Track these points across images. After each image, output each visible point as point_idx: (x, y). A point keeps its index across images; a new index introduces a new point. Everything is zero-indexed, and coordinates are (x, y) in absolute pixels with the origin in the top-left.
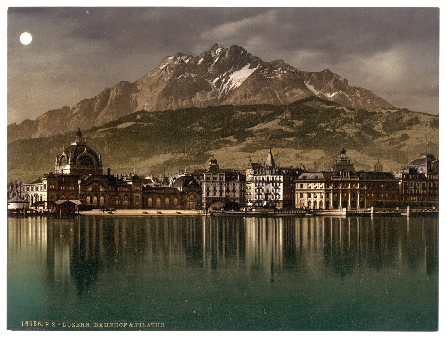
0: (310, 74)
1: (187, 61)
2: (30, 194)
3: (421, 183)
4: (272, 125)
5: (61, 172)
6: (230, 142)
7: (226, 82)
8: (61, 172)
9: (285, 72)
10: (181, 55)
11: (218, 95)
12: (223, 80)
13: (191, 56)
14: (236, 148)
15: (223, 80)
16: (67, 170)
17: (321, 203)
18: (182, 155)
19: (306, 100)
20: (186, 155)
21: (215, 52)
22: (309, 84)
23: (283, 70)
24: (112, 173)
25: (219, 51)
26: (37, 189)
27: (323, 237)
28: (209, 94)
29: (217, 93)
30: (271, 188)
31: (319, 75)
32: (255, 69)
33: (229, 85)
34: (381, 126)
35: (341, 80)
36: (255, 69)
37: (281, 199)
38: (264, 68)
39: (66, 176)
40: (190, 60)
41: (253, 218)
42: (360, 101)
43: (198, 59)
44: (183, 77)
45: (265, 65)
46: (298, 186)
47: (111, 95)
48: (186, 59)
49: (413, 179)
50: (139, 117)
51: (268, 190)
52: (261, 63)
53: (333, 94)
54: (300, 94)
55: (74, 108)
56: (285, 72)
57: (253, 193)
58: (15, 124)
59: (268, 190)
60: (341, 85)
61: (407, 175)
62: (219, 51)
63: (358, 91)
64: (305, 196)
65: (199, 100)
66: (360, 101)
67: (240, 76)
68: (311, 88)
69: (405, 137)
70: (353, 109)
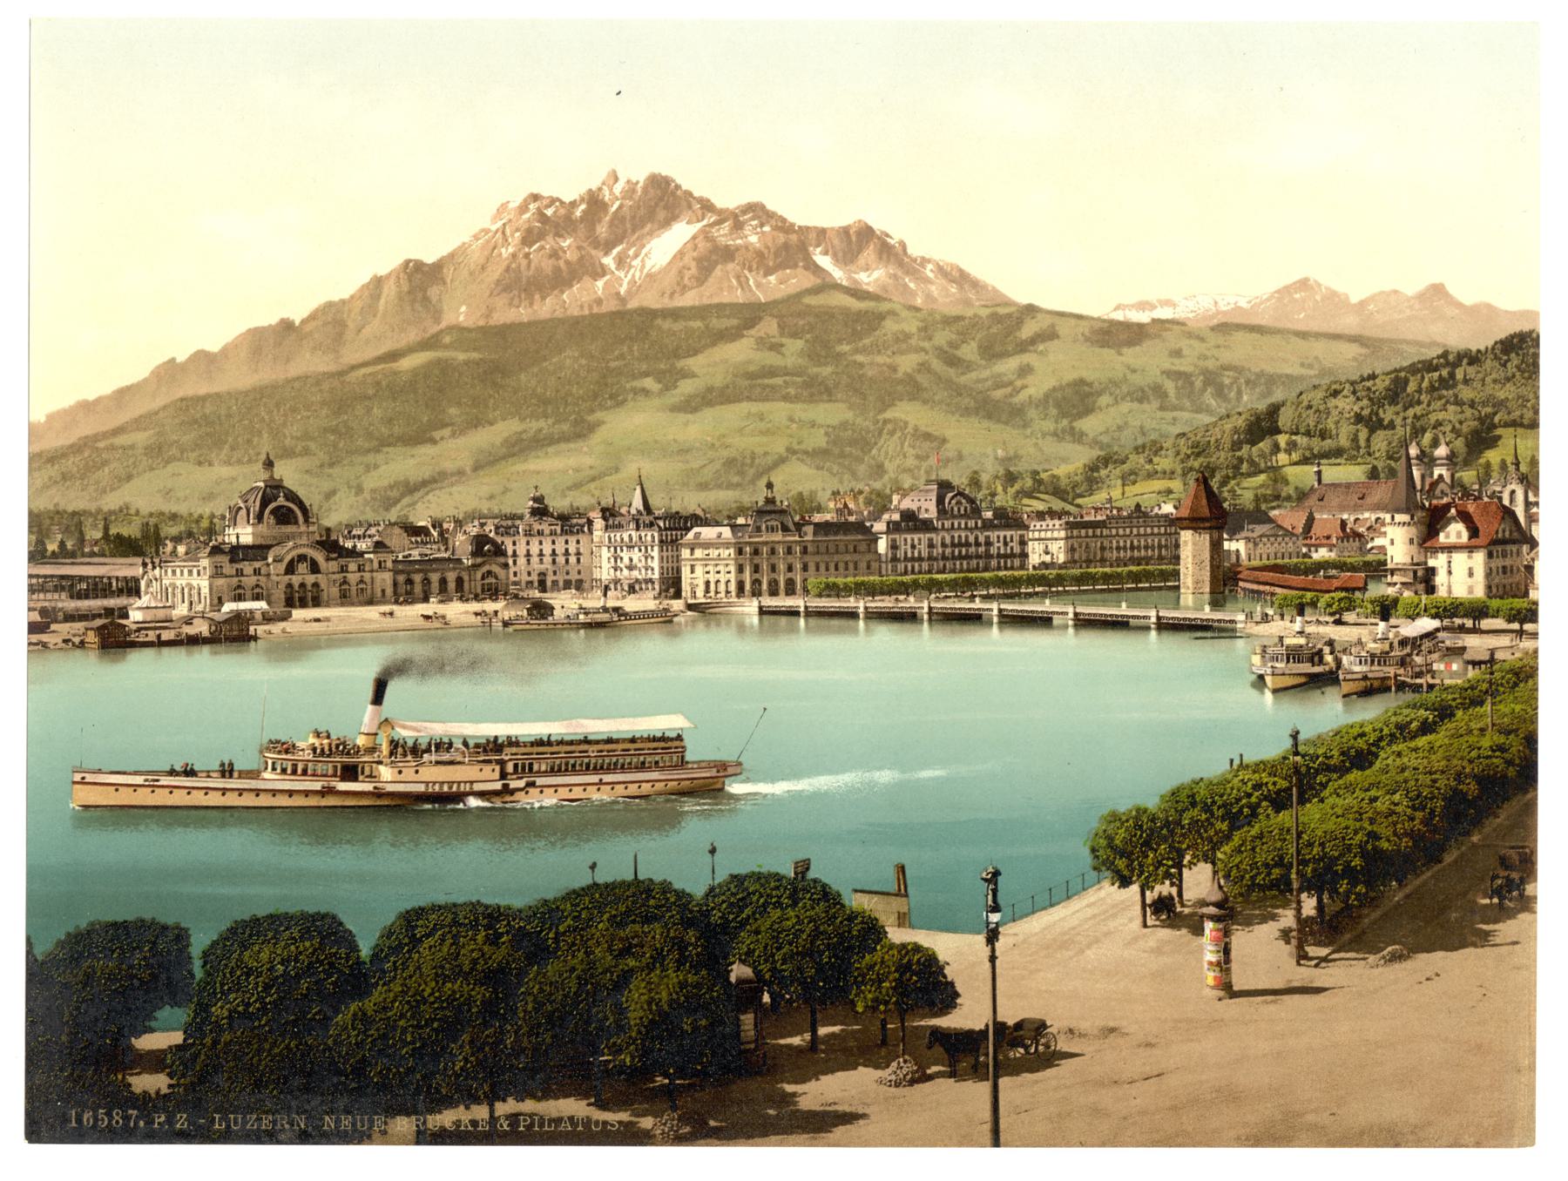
0: (822, 232)
3: (925, 537)
4: (741, 352)
6: (646, 392)
7: (636, 256)
8: (234, 540)
12: (631, 253)
14: (657, 402)
15: (631, 253)
18: (542, 423)
19: (815, 291)
20: (550, 421)
23: (762, 225)
24: (334, 537)
26: (190, 572)
27: (226, 890)
28: (600, 284)
34: (974, 345)
35: (892, 242)
36: (700, 225)
37: (656, 576)
38: (719, 222)
45: (723, 216)
46: (685, 553)
47: (385, 291)
49: (908, 530)
50: (447, 340)
54: (797, 280)
57: (605, 565)
58: (173, 360)
60: (890, 252)
61: (895, 523)
64: (699, 570)
65: (576, 299)
66: (933, 288)
67: (667, 245)
68: (824, 261)
69: (1025, 371)
70: (918, 309)
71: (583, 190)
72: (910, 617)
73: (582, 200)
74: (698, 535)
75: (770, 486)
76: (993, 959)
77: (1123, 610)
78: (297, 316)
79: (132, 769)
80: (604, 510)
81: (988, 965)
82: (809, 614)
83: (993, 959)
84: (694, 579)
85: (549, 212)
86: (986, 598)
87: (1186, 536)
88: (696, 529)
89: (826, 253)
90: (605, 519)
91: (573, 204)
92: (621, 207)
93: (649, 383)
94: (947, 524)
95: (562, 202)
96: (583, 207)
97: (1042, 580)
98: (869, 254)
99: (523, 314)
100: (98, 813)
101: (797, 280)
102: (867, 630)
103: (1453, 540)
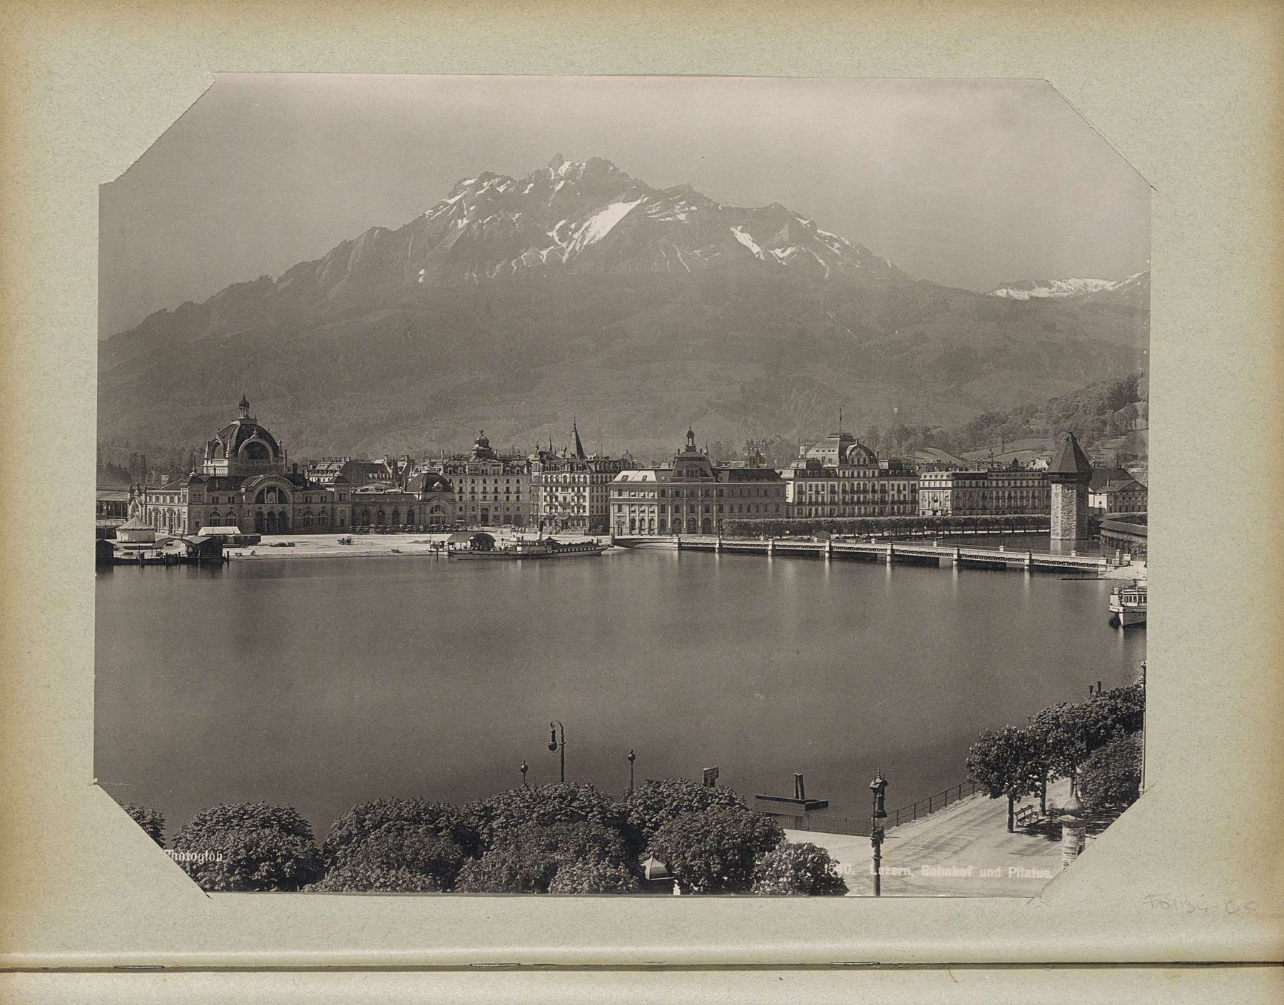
1: (501, 189)
2: (161, 508)
5: (212, 472)
8: (212, 472)
9: (693, 208)
10: (488, 176)
11: (563, 254)
13: (509, 178)
16: (222, 467)
17: (651, 520)
21: (556, 171)
22: (742, 231)
24: (299, 472)
25: (565, 167)
29: (562, 251)
30: (570, 494)
31: (762, 213)
32: (634, 204)
33: (583, 234)
36: (634, 204)
37: (587, 514)
39: (221, 478)
40: (508, 187)
41: (519, 562)
42: (840, 264)
43: (524, 183)
44: (494, 220)
45: (656, 195)
48: (499, 185)
51: (565, 498)
52: (648, 191)
53: (789, 251)
55: (281, 280)
56: (693, 208)
59: (565, 498)
62: (565, 167)
63: (837, 245)
66: (840, 264)
75: (691, 435)
77: (1001, 553)
82: (836, 556)
86: (881, 540)
87: (1056, 489)
91: (524, 183)
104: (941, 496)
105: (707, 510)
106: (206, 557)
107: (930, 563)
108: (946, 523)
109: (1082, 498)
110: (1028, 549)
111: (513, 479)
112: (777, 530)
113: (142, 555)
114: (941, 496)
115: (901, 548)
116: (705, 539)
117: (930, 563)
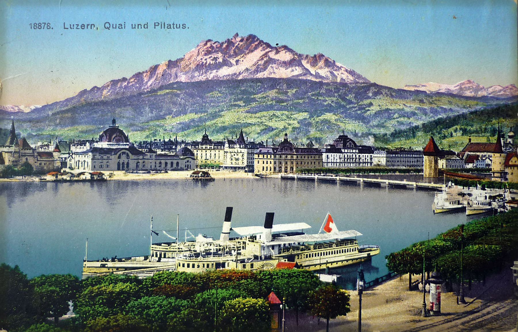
54: (297, 71)
68: (308, 66)
69: (371, 104)
71: (226, 39)
72: (333, 182)
73: (226, 41)
74: (260, 151)
75: (286, 135)
76: (360, 300)
77: (405, 182)
78: (120, 78)
79: (140, 189)
80: (228, 141)
81: (359, 302)
82: (299, 179)
83: (360, 300)
84: (258, 167)
85: (214, 46)
86: (359, 176)
87: (426, 158)
88: (260, 149)
89: (308, 62)
90: (229, 144)
91: (223, 43)
92: (239, 44)
93: (241, 103)
94: (346, 151)
95: (219, 42)
96: (226, 44)
97: (379, 171)
98: (321, 63)
99: (203, 78)
100: (472, 216)
101: (297, 71)
102: (318, 186)
103: (513, 163)
104: (381, 160)
105: (286, 163)
106: (97, 180)
107: (377, 185)
108: (383, 171)
109: (436, 162)
110: (388, 179)
111: (217, 151)
112: (318, 171)
113: (259, 157)
114: (381, 160)
115: (420, 184)
116: (291, 175)
117: (377, 185)
